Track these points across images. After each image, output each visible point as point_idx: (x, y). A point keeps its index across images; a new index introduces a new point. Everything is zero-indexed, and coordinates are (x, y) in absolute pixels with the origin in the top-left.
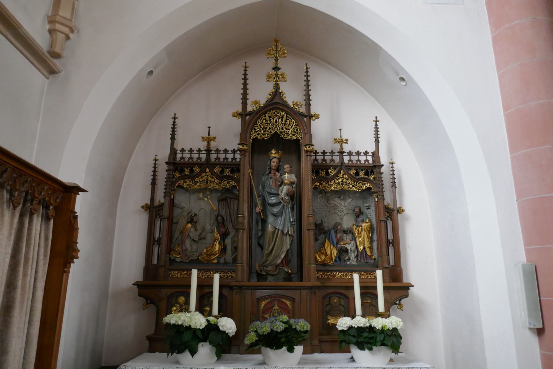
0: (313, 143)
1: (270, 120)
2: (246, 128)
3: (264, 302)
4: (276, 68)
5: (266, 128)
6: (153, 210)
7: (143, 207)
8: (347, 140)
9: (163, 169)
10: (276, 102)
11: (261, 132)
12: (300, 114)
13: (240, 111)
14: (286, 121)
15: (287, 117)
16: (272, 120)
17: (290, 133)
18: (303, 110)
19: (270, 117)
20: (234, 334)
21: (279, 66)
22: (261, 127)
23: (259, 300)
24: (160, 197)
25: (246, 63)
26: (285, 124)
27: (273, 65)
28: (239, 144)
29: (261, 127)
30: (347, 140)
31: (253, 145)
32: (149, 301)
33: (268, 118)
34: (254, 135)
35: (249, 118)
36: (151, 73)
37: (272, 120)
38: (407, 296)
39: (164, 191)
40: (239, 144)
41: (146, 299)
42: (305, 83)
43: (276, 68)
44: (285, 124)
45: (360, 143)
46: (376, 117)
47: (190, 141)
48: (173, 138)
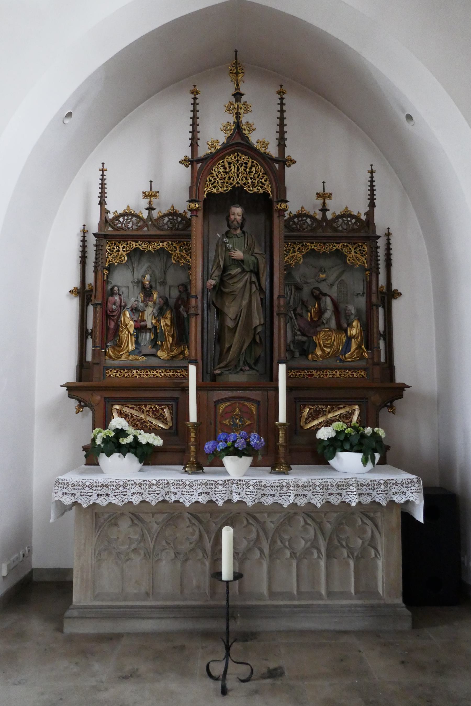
0: (288, 199)
1: (230, 167)
2: (197, 181)
3: (222, 406)
4: (238, 95)
5: (224, 178)
6: (83, 294)
7: (71, 292)
8: (331, 194)
9: (92, 241)
10: (238, 142)
11: (218, 183)
12: (269, 158)
13: (190, 156)
14: (251, 168)
15: (253, 162)
16: (233, 167)
17: (256, 184)
18: (273, 151)
19: (230, 163)
20: (159, 438)
21: (242, 91)
22: (218, 177)
23: (217, 403)
24: (90, 278)
25: (195, 86)
26: (250, 172)
27: (233, 91)
28: (190, 201)
29: (218, 177)
30: (331, 194)
31: (205, 202)
32: (83, 404)
33: (227, 166)
34: (206, 190)
35: (199, 165)
36: (70, 115)
37: (233, 167)
38: (401, 396)
39: (94, 264)
40: (190, 201)
41: (80, 401)
42: (278, 114)
43: (238, 95)
44: (250, 172)
45: (349, 199)
46: (372, 165)
47: (125, 197)
48: (102, 203)
